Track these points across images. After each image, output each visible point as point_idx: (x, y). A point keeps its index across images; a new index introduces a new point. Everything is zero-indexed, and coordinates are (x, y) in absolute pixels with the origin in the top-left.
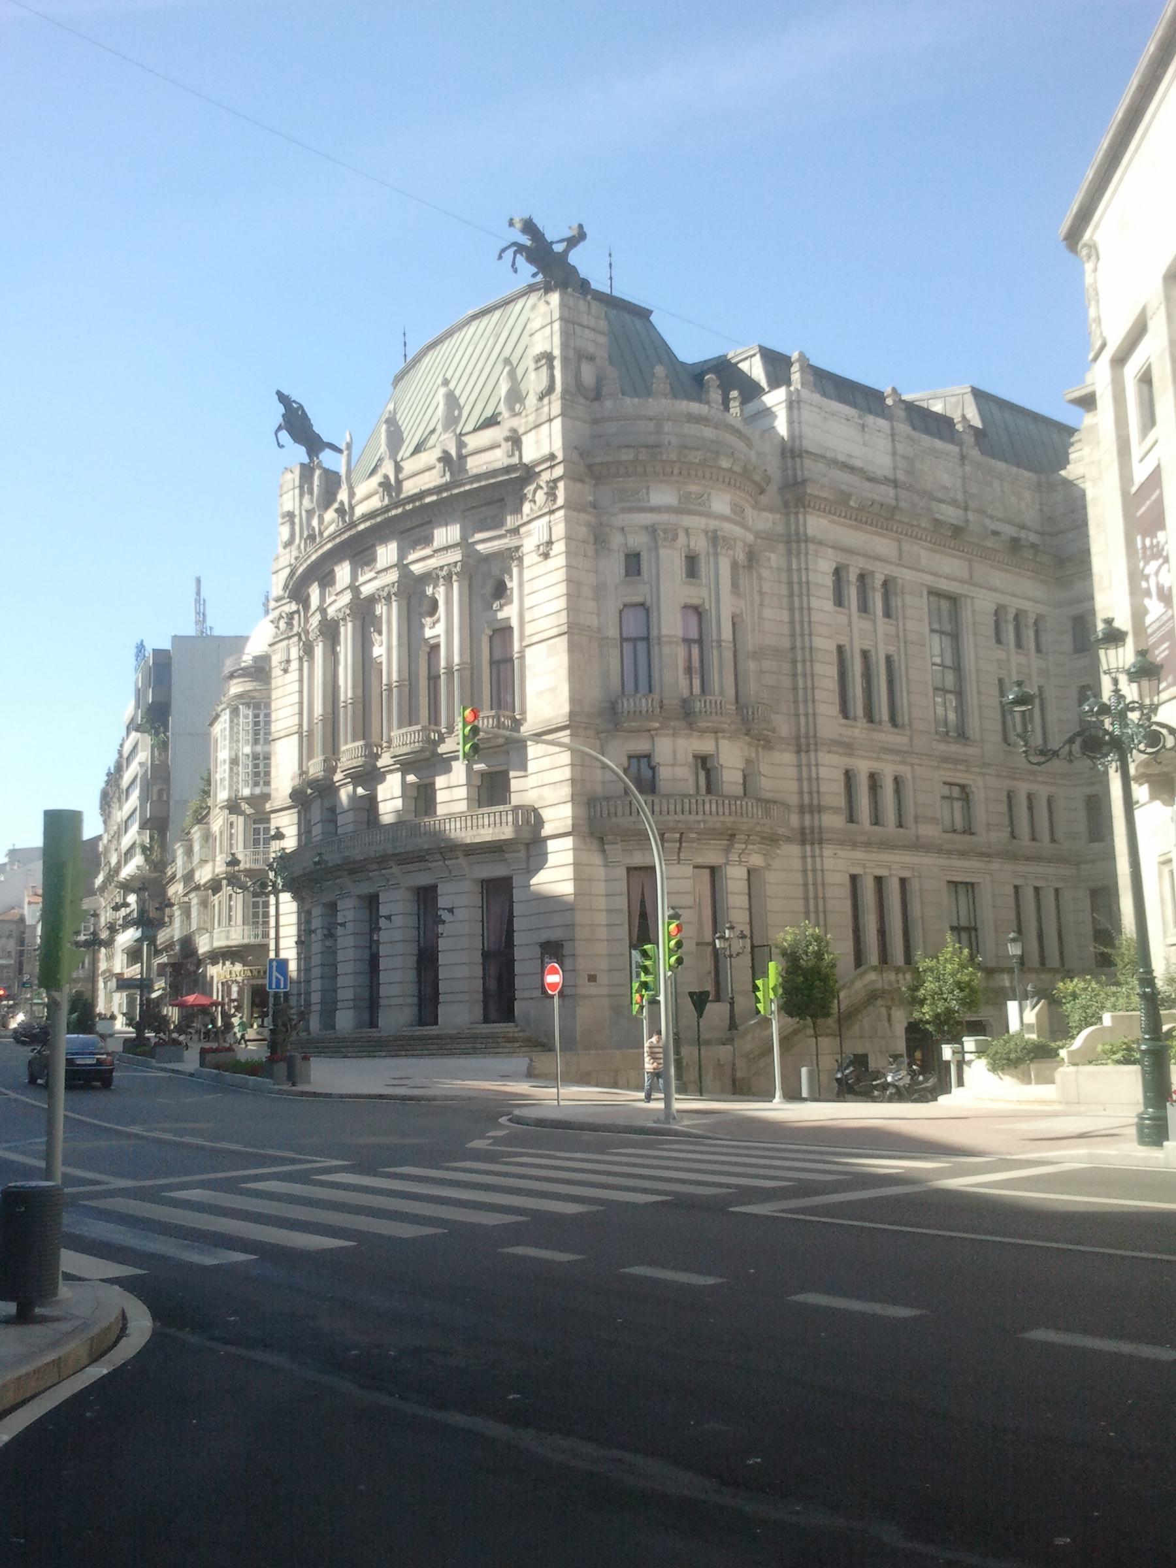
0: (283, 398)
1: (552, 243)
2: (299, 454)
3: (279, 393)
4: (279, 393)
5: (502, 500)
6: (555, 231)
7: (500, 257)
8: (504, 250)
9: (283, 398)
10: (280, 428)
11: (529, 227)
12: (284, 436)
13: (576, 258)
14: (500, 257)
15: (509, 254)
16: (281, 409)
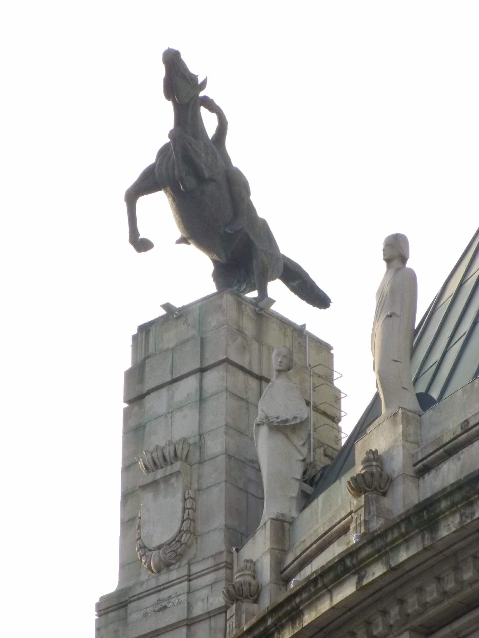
0: (181, 85)
2: (188, 274)
3: (173, 61)
4: (173, 61)
9: (181, 85)
10: (147, 183)
12: (159, 212)
16: (159, 121)
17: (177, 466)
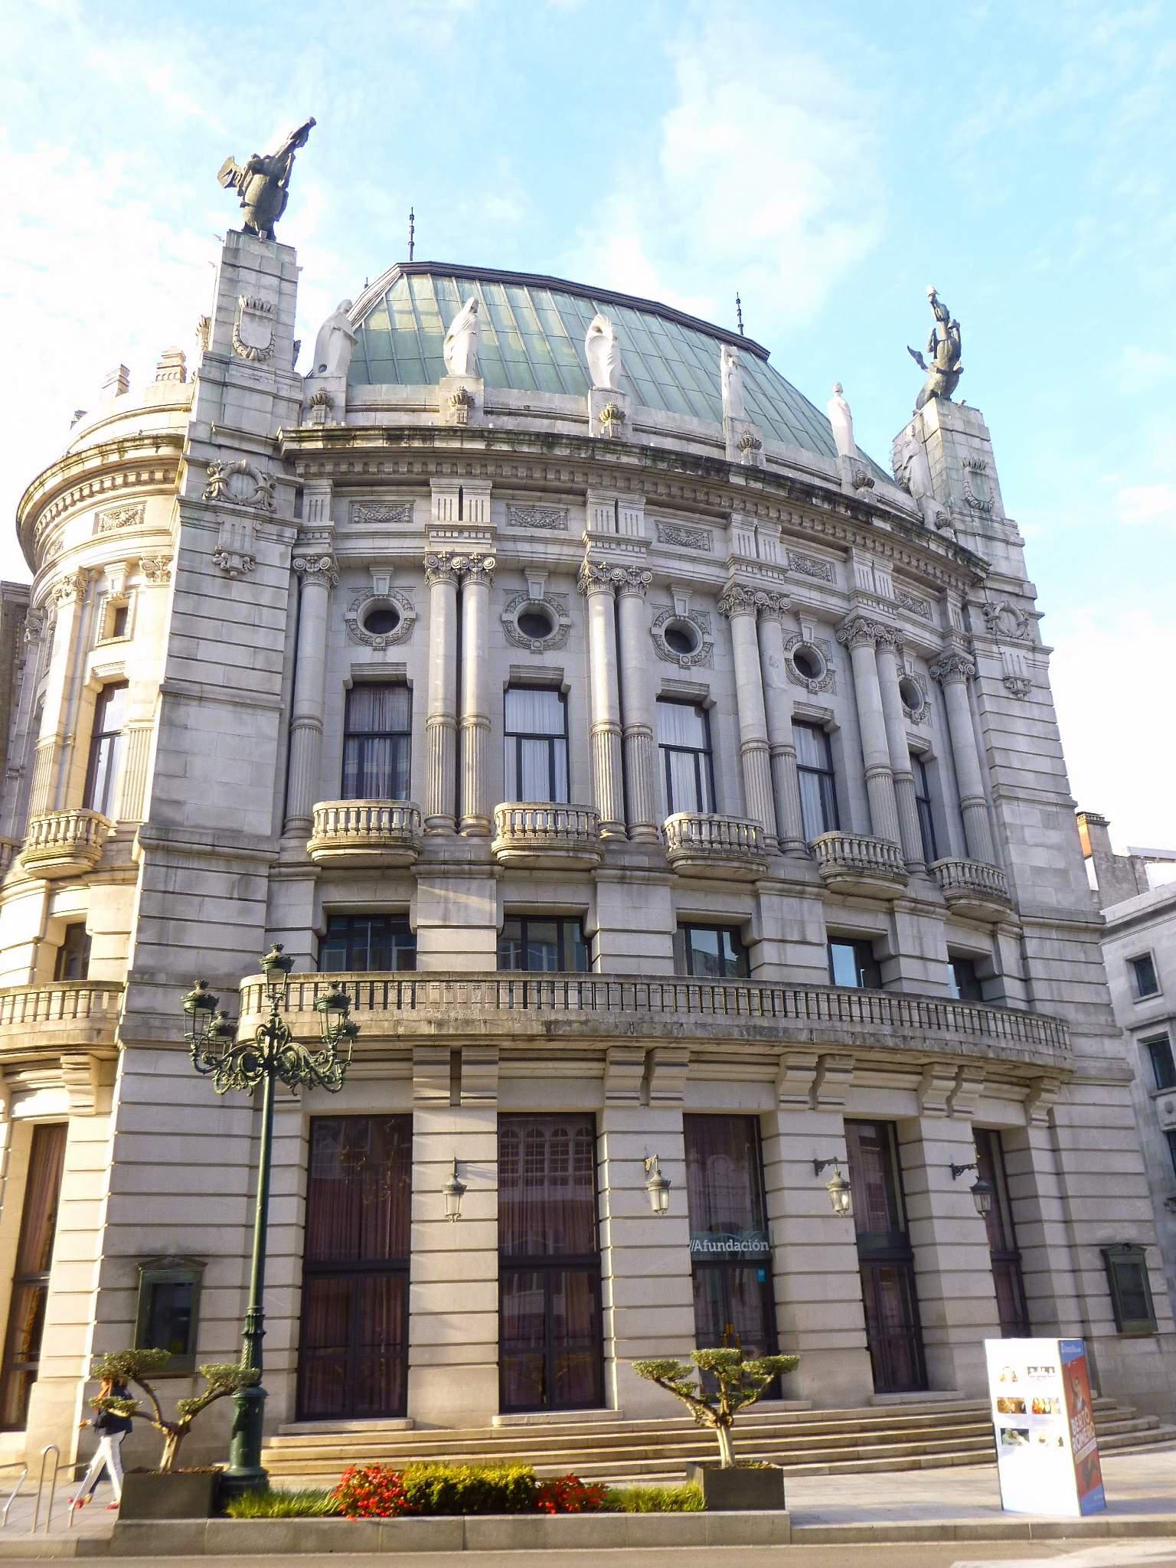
5: (427, 484)
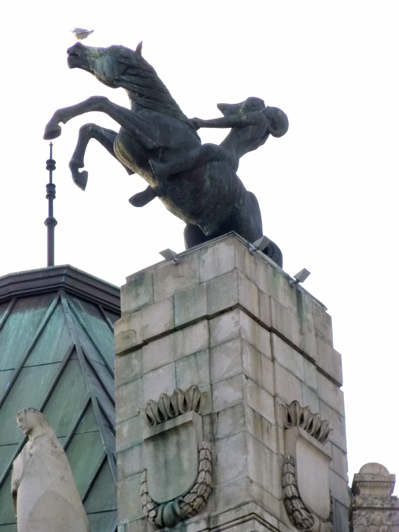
0: (92, 32)
1: (197, 124)
6: (199, 95)
7: (52, 132)
8: (64, 115)
9: (92, 32)
11: (127, 68)
13: (254, 170)
14: (52, 132)
15: (71, 129)
16: (90, 30)
17: (189, 416)
